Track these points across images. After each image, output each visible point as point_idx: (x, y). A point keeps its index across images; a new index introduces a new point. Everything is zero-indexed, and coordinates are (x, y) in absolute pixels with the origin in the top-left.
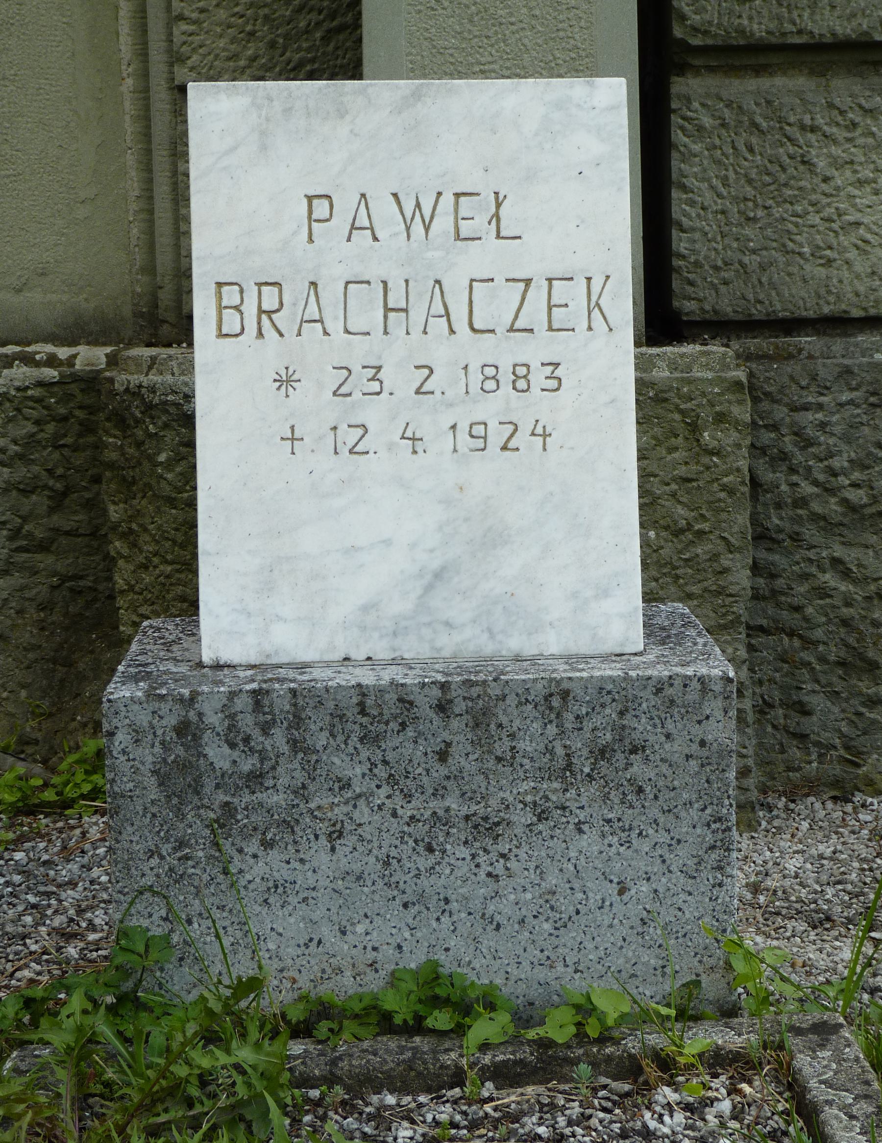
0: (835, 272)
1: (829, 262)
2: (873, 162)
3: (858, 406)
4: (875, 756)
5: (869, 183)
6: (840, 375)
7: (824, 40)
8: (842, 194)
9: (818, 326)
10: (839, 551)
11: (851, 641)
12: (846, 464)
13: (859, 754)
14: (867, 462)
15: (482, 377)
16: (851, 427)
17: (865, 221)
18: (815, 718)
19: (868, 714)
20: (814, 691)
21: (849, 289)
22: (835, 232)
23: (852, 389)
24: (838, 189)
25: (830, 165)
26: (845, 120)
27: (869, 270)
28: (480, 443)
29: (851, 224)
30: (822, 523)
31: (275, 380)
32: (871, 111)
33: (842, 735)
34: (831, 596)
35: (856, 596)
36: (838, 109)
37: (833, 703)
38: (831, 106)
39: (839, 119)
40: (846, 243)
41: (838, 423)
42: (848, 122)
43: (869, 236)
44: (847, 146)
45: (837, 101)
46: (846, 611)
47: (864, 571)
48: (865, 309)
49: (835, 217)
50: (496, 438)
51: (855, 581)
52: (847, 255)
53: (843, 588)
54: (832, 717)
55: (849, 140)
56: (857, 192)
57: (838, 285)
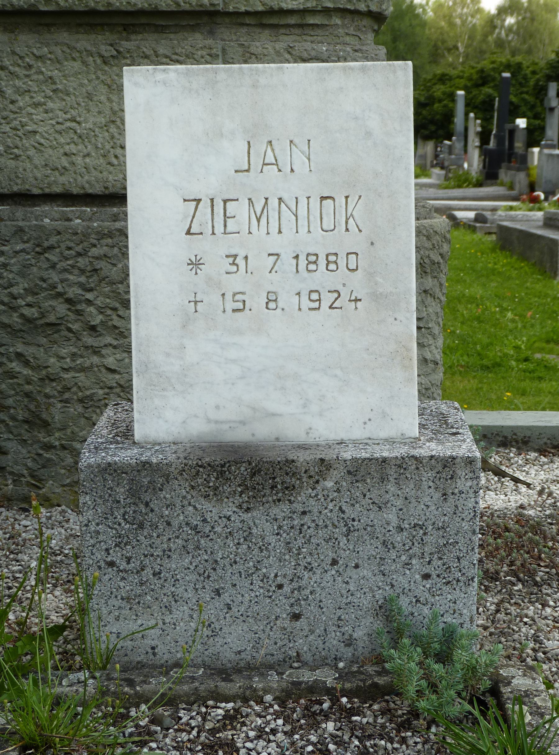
0: (21, 164)
1: (17, 157)
2: (44, 91)
3: (28, 253)
4: (51, 482)
5: (41, 106)
6: (16, 233)
7: (6, 9)
8: (23, 112)
9: (15, 199)
10: (20, 348)
11: (32, 407)
12: (22, 291)
13: (40, 481)
14: (36, 290)
15: (307, 262)
16: (24, 267)
17: (40, 130)
18: (9, 457)
19: (45, 455)
20: (9, 439)
21: (31, 175)
22: (19, 137)
23: (25, 242)
24: (20, 108)
25: (15, 92)
26: (23, 63)
27: (44, 163)
29: (30, 132)
30: (9, 330)
31: (188, 264)
32: (40, 57)
33: (28, 469)
34: (17, 378)
35: (33, 378)
36: (18, 55)
37: (23, 447)
38: (14, 53)
39: (20, 62)
40: (27, 145)
41: (14, 264)
42: (26, 64)
43: (42, 141)
44: (26, 80)
45: (18, 50)
46: (28, 388)
47: (37, 362)
48: (41, 189)
49: (19, 127)
51: (33, 368)
52: (28, 153)
53: (25, 372)
54: (21, 456)
55: (27, 76)
56: (33, 111)
57: (23, 172)
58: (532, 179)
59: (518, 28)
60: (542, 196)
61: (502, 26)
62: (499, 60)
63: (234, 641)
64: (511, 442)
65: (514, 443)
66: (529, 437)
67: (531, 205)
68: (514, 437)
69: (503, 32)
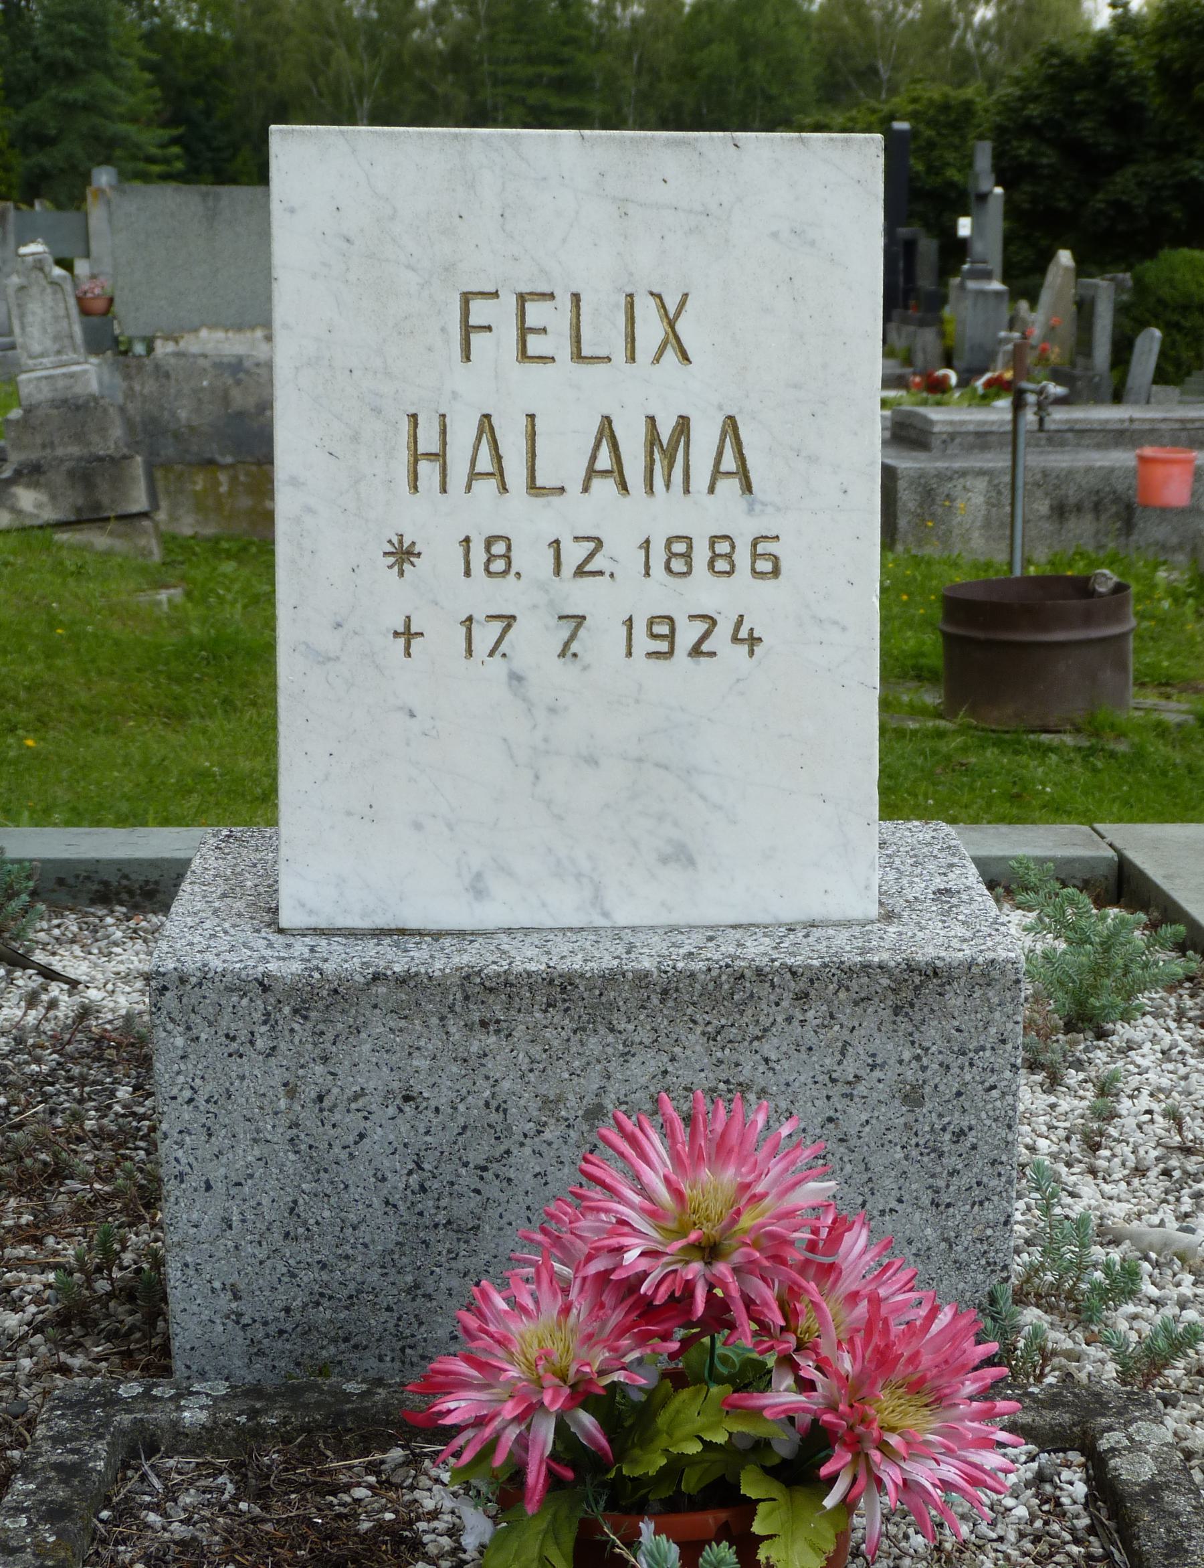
28: (663, 646)
50: (688, 635)
58: (949, 342)
59: (1000, 32)
60: (953, 378)
61: (968, 24)
62: (927, 95)
64: (118, 893)
65: (125, 896)
66: (156, 883)
67: (925, 395)
68: (124, 882)
69: (969, 36)
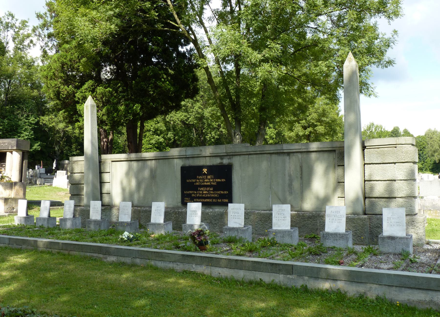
63: (390, 251)
